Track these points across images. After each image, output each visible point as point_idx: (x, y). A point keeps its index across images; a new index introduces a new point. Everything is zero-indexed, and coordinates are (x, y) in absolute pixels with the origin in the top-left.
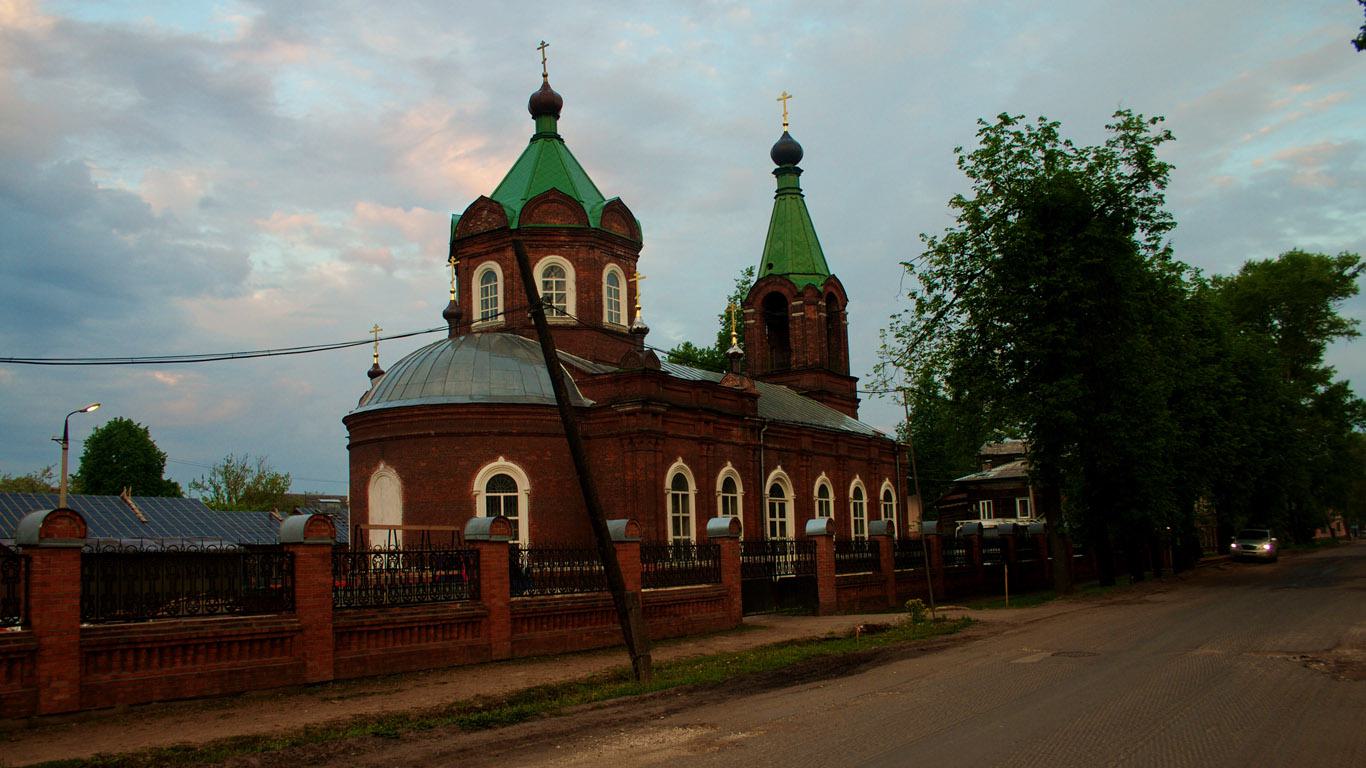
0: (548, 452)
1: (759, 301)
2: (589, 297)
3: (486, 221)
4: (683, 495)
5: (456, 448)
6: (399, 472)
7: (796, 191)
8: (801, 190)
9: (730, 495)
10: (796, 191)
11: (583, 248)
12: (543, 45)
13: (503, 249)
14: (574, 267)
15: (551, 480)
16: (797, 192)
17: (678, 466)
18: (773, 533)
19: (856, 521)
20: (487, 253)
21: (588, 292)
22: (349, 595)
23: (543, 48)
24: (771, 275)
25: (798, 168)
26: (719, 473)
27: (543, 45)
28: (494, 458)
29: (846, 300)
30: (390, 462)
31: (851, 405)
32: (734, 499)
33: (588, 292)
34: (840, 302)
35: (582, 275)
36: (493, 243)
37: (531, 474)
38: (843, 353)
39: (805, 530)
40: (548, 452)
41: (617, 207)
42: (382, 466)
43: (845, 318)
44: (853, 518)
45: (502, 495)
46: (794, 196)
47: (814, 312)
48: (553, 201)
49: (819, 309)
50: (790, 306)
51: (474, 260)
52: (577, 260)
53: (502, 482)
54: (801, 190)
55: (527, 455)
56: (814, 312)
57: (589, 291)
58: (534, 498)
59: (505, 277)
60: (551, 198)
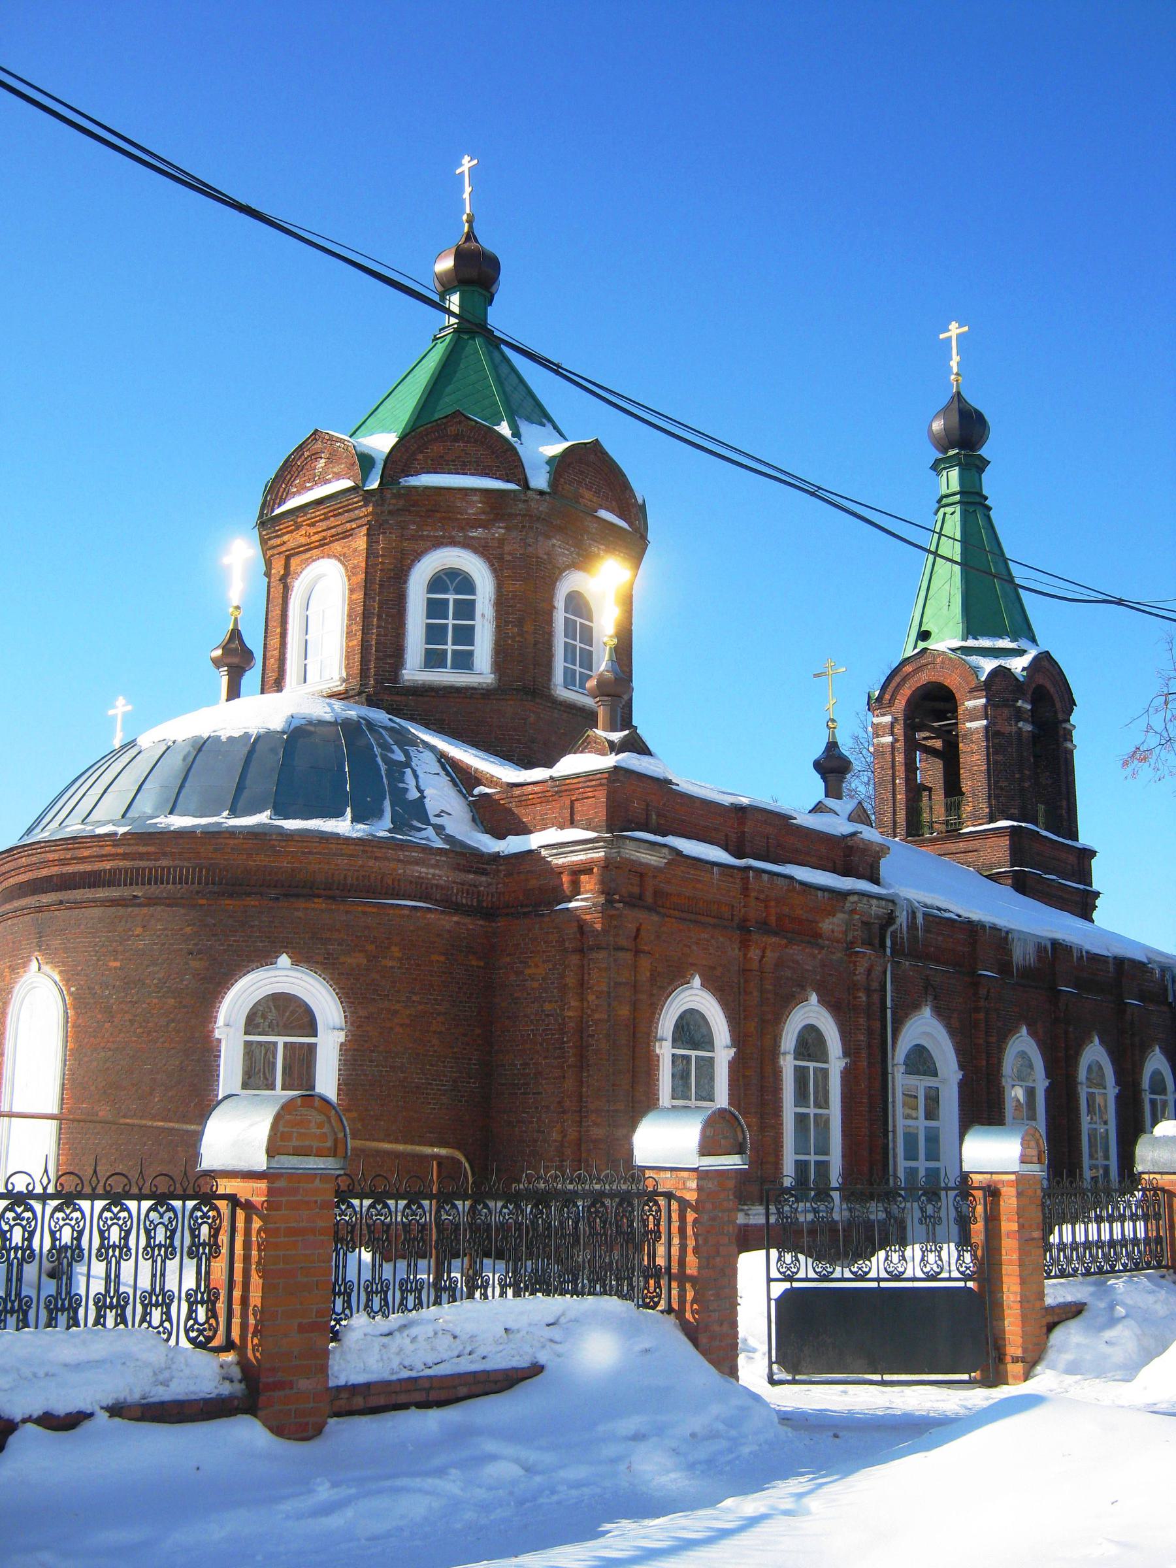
0: (394, 949)
1: (900, 703)
7: (978, 499)
8: (986, 498)
9: (811, 1065)
10: (978, 499)
11: (514, 534)
13: (347, 535)
15: (396, 1012)
17: (695, 997)
18: (911, 1155)
19: (801, 1119)
20: (322, 544)
22: (115, 1235)
24: (925, 650)
26: (960, 1051)
29: (1070, 703)
30: (52, 956)
31: (1083, 904)
32: (707, 1065)
33: (520, 623)
34: (1058, 705)
36: (332, 522)
38: (1064, 803)
39: (196, 1156)
41: (592, 457)
42: (34, 965)
44: (789, 1109)
45: (281, 1040)
47: (1009, 719)
48: (457, 438)
49: (1019, 715)
50: (960, 710)
52: (501, 558)
53: (288, 1013)
54: (986, 498)
56: (1009, 719)
60: (452, 430)
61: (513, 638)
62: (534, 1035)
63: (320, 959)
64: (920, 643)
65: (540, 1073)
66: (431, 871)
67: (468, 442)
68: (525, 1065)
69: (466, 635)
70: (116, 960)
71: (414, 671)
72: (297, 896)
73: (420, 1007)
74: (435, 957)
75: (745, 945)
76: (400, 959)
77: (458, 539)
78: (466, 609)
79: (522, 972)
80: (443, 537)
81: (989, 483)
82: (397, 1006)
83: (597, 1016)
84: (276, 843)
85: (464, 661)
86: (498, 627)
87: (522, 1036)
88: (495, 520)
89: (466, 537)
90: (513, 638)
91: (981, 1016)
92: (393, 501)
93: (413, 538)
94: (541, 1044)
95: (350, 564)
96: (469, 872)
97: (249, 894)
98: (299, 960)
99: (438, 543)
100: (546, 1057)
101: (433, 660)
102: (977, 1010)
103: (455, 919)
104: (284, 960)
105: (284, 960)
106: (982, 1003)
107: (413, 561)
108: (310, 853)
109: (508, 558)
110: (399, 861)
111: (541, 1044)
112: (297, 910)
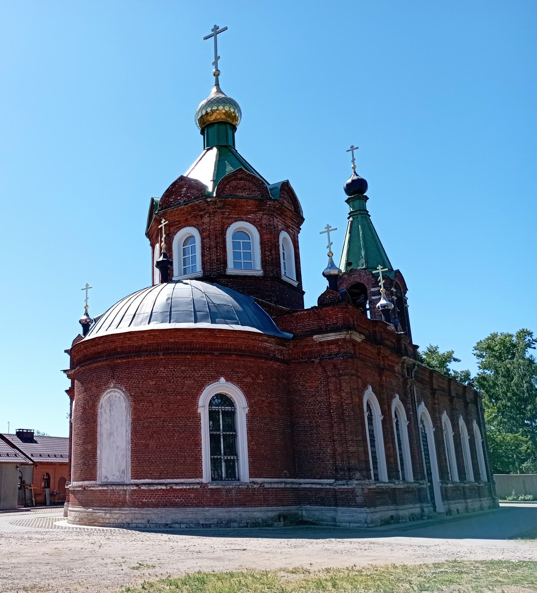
2: (271, 255)
3: (185, 195)
4: (225, 413)
5: (184, 368)
6: (128, 390)
7: (366, 213)
10: (366, 213)
11: (265, 216)
12: (87, 287)
14: (259, 231)
15: (263, 401)
16: (365, 214)
21: (270, 250)
23: (87, 289)
24: (351, 270)
25: (366, 196)
27: (87, 287)
28: (215, 379)
33: (270, 250)
35: (266, 237)
37: (248, 395)
40: (261, 376)
43: (406, 303)
46: (364, 216)
48: (241, 179)
50: (368, 292)
51: (175, 227)
52: (261, 226)
55: (244, 377)
57: (270, 248)
58: (251, 418)
59: (203, 239)
60: (239, 176)
61: (268, 256)
62: (314, 410)
63: (236, 379)
64: (348, 267)
65: (319, 426)
66: (269, 345)
67: (245, 181)
68: (311, 422)
69: (248, 256)
70: (152, 381)
71: (231, 270)
72: (226, 354)
73: (271, 399)
74: (273, 379)
75: (380, 375)
76: (263, 380)
77: (244, 218)
78: (248, 246)
79: (305, 385)
80: (238, 218)
81: (369, 206)
82: (263, 399)
83: (347, 402)
84: (216, 333)
85: (249, 266)
86: (262, 252)
87: (308, 411)
88: (258, 211)
89: (247, 217)
90: (268, 256)
91: (437, 406)
92: (219, 203)
93: (227, 218)
94: (318, 414)
95: (201, 228)
96: (281, 345)
97: (207, 354)
98: (229, 379)
99: (236, 220)
100: (321, 419)
101: (237, 265)
102: (435, 404)
103: (278, 364)
104: (222, 380)
105: (222, 380)
106: (436, 401)
107: (227, 227)
108: (229, 337)
109: (264, 226)
110: (260, 340)
111: (318, 414)
112: (225, 360)
